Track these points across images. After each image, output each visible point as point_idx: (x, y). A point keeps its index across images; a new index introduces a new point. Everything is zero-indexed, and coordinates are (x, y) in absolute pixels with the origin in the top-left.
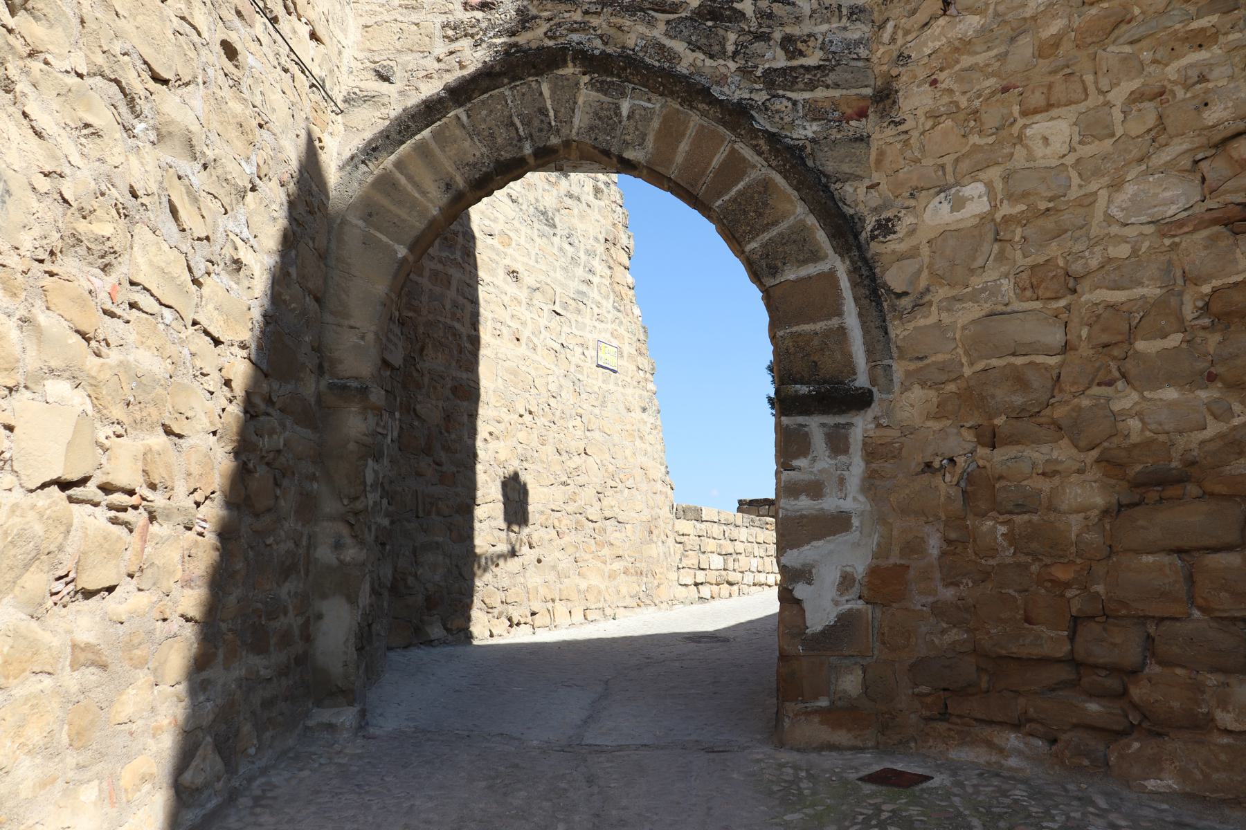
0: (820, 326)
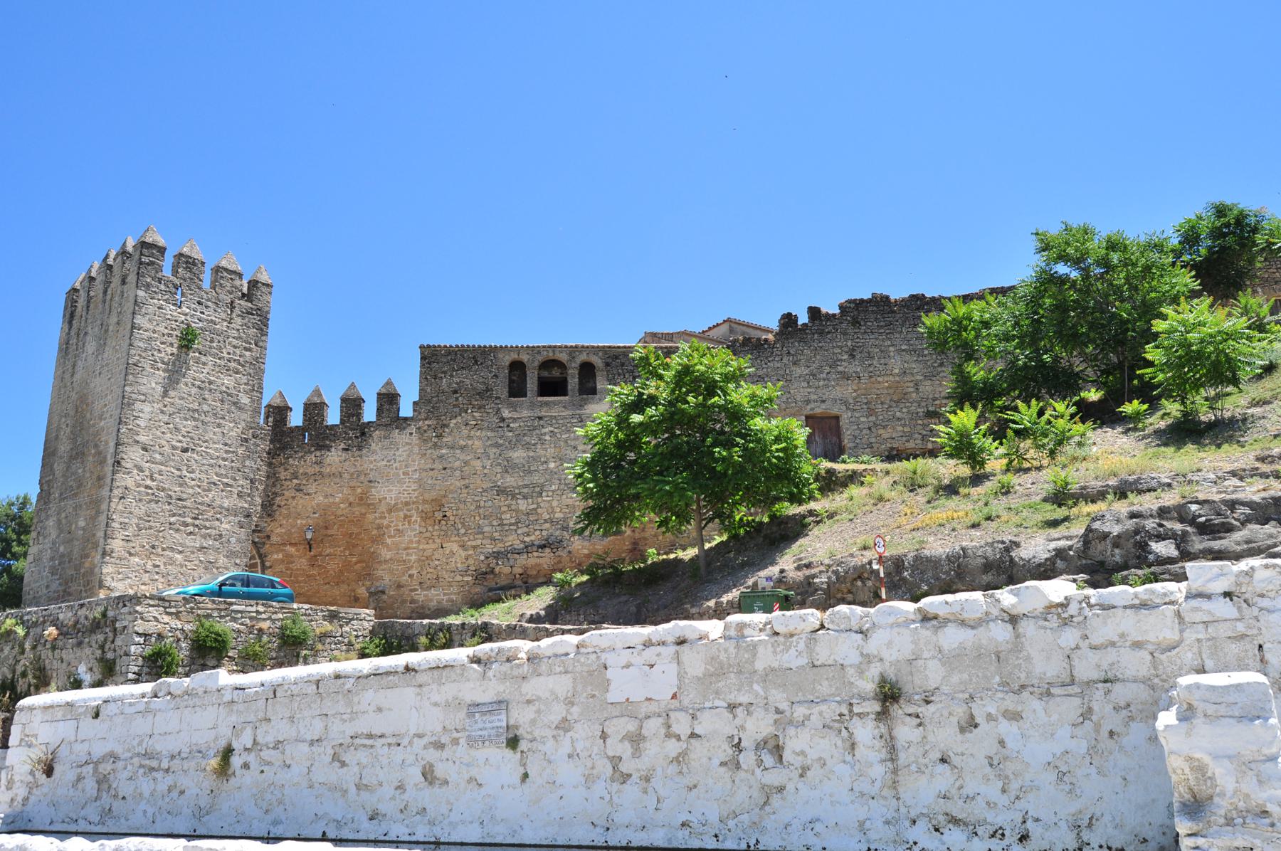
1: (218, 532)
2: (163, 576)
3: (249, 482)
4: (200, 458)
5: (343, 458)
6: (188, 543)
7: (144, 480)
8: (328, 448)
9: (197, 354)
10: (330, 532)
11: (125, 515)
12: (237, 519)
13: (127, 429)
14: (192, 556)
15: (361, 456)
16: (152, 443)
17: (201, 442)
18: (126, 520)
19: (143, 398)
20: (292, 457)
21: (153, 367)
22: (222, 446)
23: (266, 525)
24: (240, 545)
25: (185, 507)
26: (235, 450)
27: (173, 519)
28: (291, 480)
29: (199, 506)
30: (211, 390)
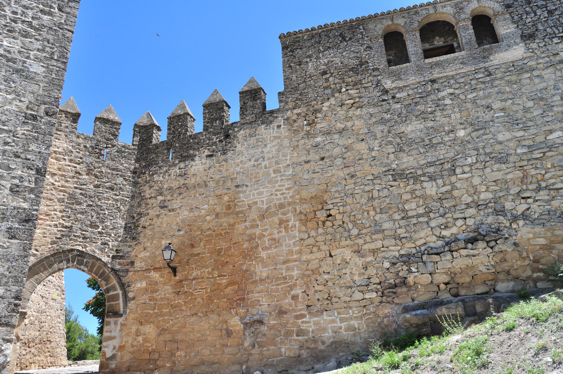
5: (208, 166)
8: (192, 158)
10: (196, 251)
15: (226, 161)
20: (156, 173)
23: (130, 249)
28: (155, 198)
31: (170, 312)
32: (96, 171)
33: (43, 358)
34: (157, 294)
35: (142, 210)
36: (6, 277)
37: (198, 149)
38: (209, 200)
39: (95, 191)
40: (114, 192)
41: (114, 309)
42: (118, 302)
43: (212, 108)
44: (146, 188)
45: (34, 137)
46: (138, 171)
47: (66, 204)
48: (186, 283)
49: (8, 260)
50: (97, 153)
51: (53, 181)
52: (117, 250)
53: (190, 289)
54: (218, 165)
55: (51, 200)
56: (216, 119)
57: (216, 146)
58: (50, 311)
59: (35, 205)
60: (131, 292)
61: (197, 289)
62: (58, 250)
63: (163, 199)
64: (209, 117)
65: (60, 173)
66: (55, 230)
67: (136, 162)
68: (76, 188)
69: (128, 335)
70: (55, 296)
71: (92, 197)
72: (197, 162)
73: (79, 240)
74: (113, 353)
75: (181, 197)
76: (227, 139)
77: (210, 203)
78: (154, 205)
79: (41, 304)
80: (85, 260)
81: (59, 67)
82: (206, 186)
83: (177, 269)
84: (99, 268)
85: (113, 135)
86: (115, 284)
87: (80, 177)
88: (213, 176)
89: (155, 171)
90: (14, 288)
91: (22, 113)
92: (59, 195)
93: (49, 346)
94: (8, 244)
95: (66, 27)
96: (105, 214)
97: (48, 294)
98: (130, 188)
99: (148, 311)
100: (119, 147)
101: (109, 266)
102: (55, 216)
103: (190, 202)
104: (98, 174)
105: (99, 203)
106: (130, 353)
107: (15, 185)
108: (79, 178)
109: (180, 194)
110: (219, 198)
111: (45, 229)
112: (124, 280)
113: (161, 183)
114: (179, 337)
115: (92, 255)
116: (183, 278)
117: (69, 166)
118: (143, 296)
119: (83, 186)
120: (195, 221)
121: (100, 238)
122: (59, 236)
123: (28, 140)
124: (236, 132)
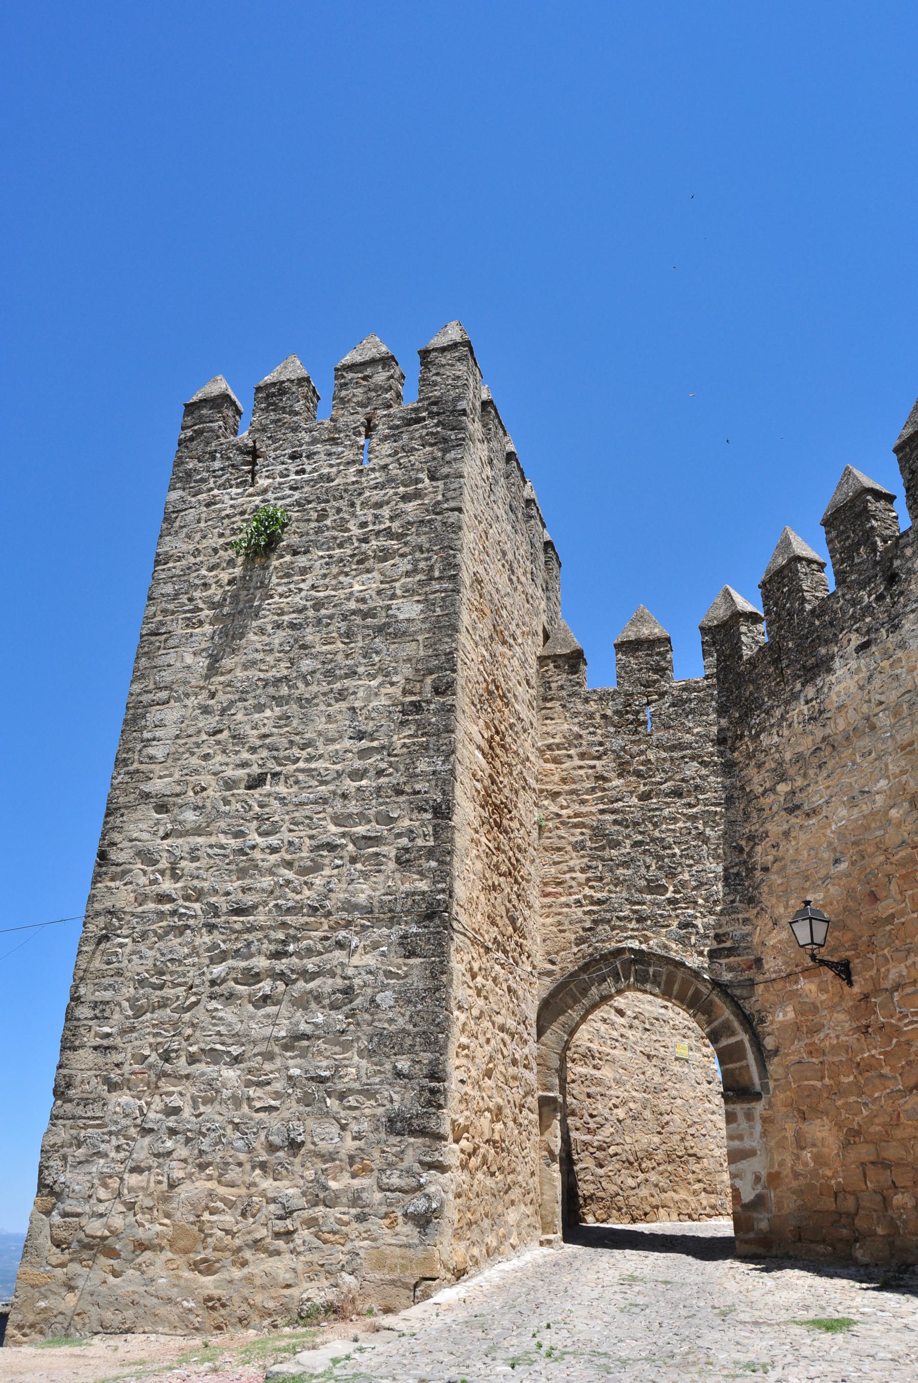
0: (738, 1065)
1: (339, 982)
2: (188, 1140)
3: (428, 816)
4: (295, 789)
5: (864, 674)
6: (257, 1030)
7: (154, 882)
8: (824, 665)
9: (288, 558)
10: (885, 908)
11: (106, 981)
12: (396, 931)
13: (127, 773)
14: (268, 1066)
15: (902, 645)
16: (178, 789)
17: (296, 752)
18: (108, 995)
19: (164, 695)
20: (763, 730)
21: (188, 623)
22: (347, 743)
23: (747, 929)
24: (408, 1011)
25: (250, 929)
26: (385, 741)
27: (218, 970)
28: (773, 790)
29: (288, 919)
30: (319, 621)
31: (856, 1083)
32: (635, 765)
33: (683, 1195)
34: (822, 1035)
35: (753, 827)
36: (409, 1035)
37: (835, 640)
38: (886, 765)
39: (642, 809)
40: (684, 801)
41: (737, 1082)
42: (744, 1063)
43: (841, 523)
44: (752, 771)
45: (421, 745)
46: (730, 734)
47: (590, 852)
48: (878, 1000)
49: (410, 1002)
50: (631, 723)
51: (556, 809)
52: (717, 936)
53: (892, 1017)
54: (886, 664)
55: (559, 849)
56: (859, 544)
57: (872, 615)
58: (677, 1086)
59: (439, 882)
60: (769, 1034)
61: (906, 1016)
62: (591, 955)
63: (789, 789)
64: (842, 547)
65: (566, 788)
66: (579, 912)
67: (719, 716)
68: (602, 812)
69: (781, 1145)
70: (683, 1052)
71: (638, 824)
72: (839, 673)
73: (630, 926)
74: (757, 1192)
75: (825, 773)
76: (892, 586)
77: (890, 772)
78: (775, 808)
79: (648, 1074)
80: (651, 970)
81: (445, 591)
82: (873, 728)
83: (851, 965)
84: (685, 984)
85: (656, 671)
86: (728, 1020)
87: (606, 785)
88: (883, 698)
89: (760, 724)
90: (426, 1057)
91: (397, 705)
92: (573, 835)
93: (696, 1167)
94: (405, 969)
95: (446, 506)
96: (674, 855)
97: (662, 1049)
98: (719, 780)
99: (811, 1083)
100: (675, 693)
101: (706, 976)
102: (574, 883)
103: (846, 780)
104: (641, 768)
105: (657, 834)
106: (793, 1193)
107: (403, 849)
108: (604, 790)
109: (820, 767)
110: (910, 753)
111: (560, 914)
112: (749, 1007)
113: (777, 751)
114: (892, 1152)
115: (663, 957)
116: (869, 988)
117: (581, 767)
118: (793, 1044)
119: (615, 805)
120: (867, 828)
121: (673, 914)
122: (588, 925)
123: (413, 754)
124: (910, 558)
